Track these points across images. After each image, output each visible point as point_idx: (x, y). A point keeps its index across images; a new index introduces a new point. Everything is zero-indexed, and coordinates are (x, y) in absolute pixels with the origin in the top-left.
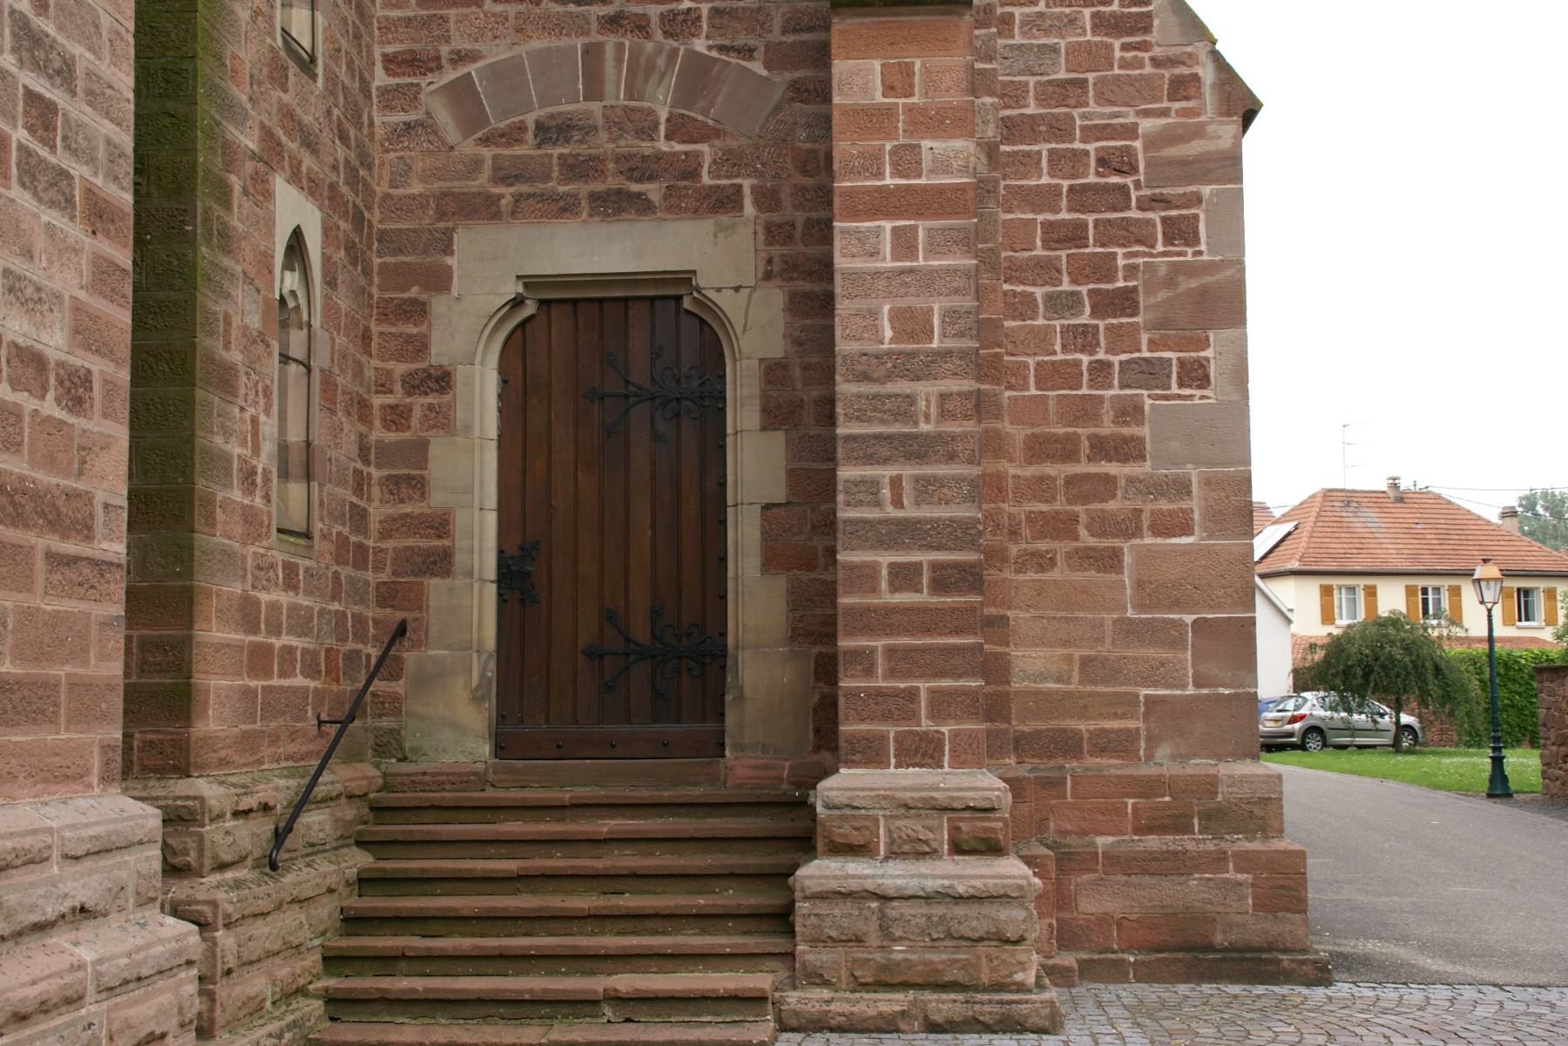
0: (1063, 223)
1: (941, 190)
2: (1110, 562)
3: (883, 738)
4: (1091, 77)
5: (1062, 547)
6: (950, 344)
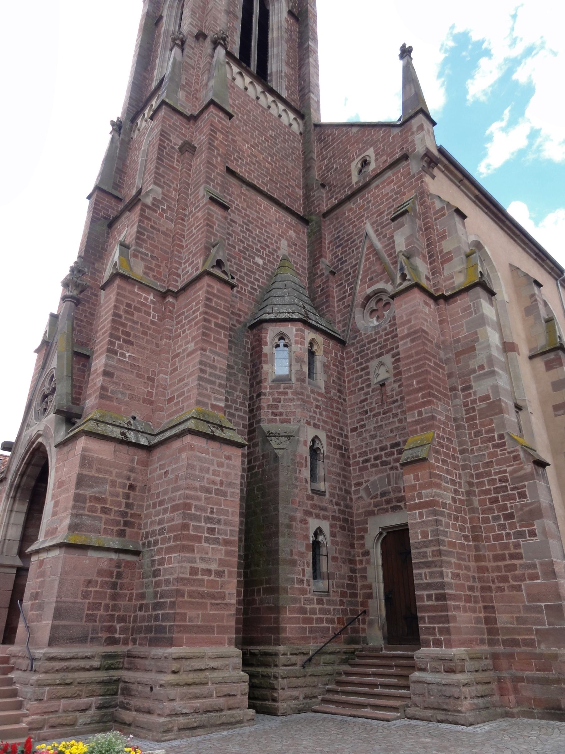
0: (493, 497)
1: (426, 502)
2: (519, 588)
3: (429, 639)
4: (494, 460)
5: (506, 585)
6: (433, 538)
